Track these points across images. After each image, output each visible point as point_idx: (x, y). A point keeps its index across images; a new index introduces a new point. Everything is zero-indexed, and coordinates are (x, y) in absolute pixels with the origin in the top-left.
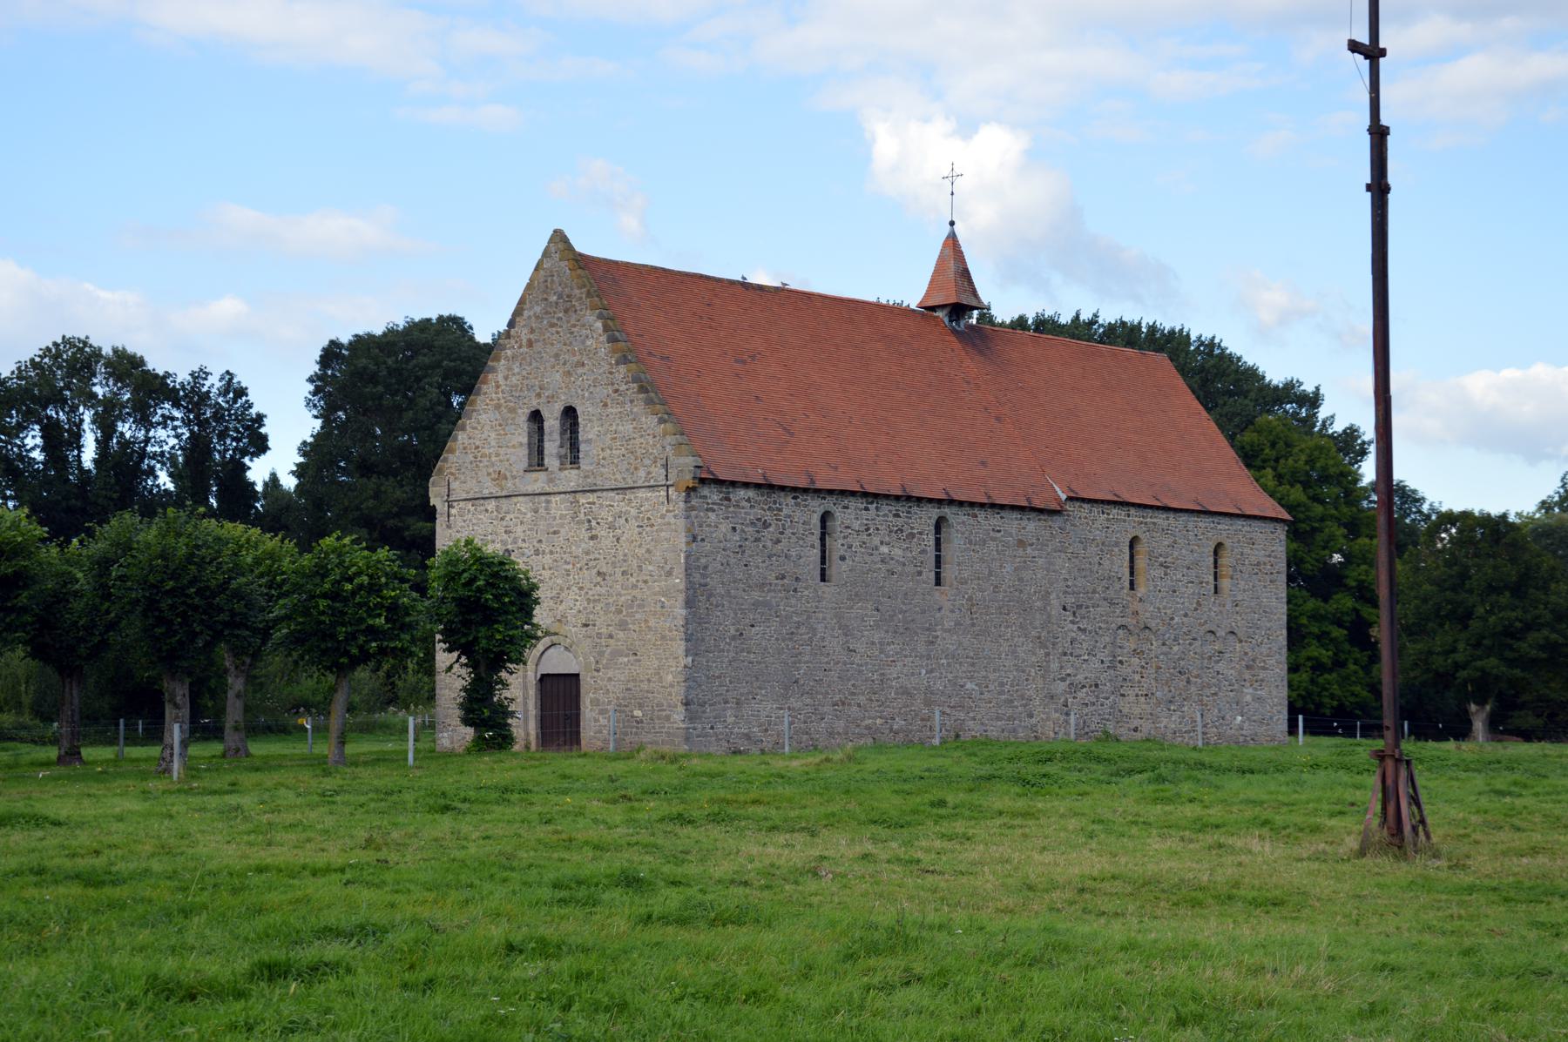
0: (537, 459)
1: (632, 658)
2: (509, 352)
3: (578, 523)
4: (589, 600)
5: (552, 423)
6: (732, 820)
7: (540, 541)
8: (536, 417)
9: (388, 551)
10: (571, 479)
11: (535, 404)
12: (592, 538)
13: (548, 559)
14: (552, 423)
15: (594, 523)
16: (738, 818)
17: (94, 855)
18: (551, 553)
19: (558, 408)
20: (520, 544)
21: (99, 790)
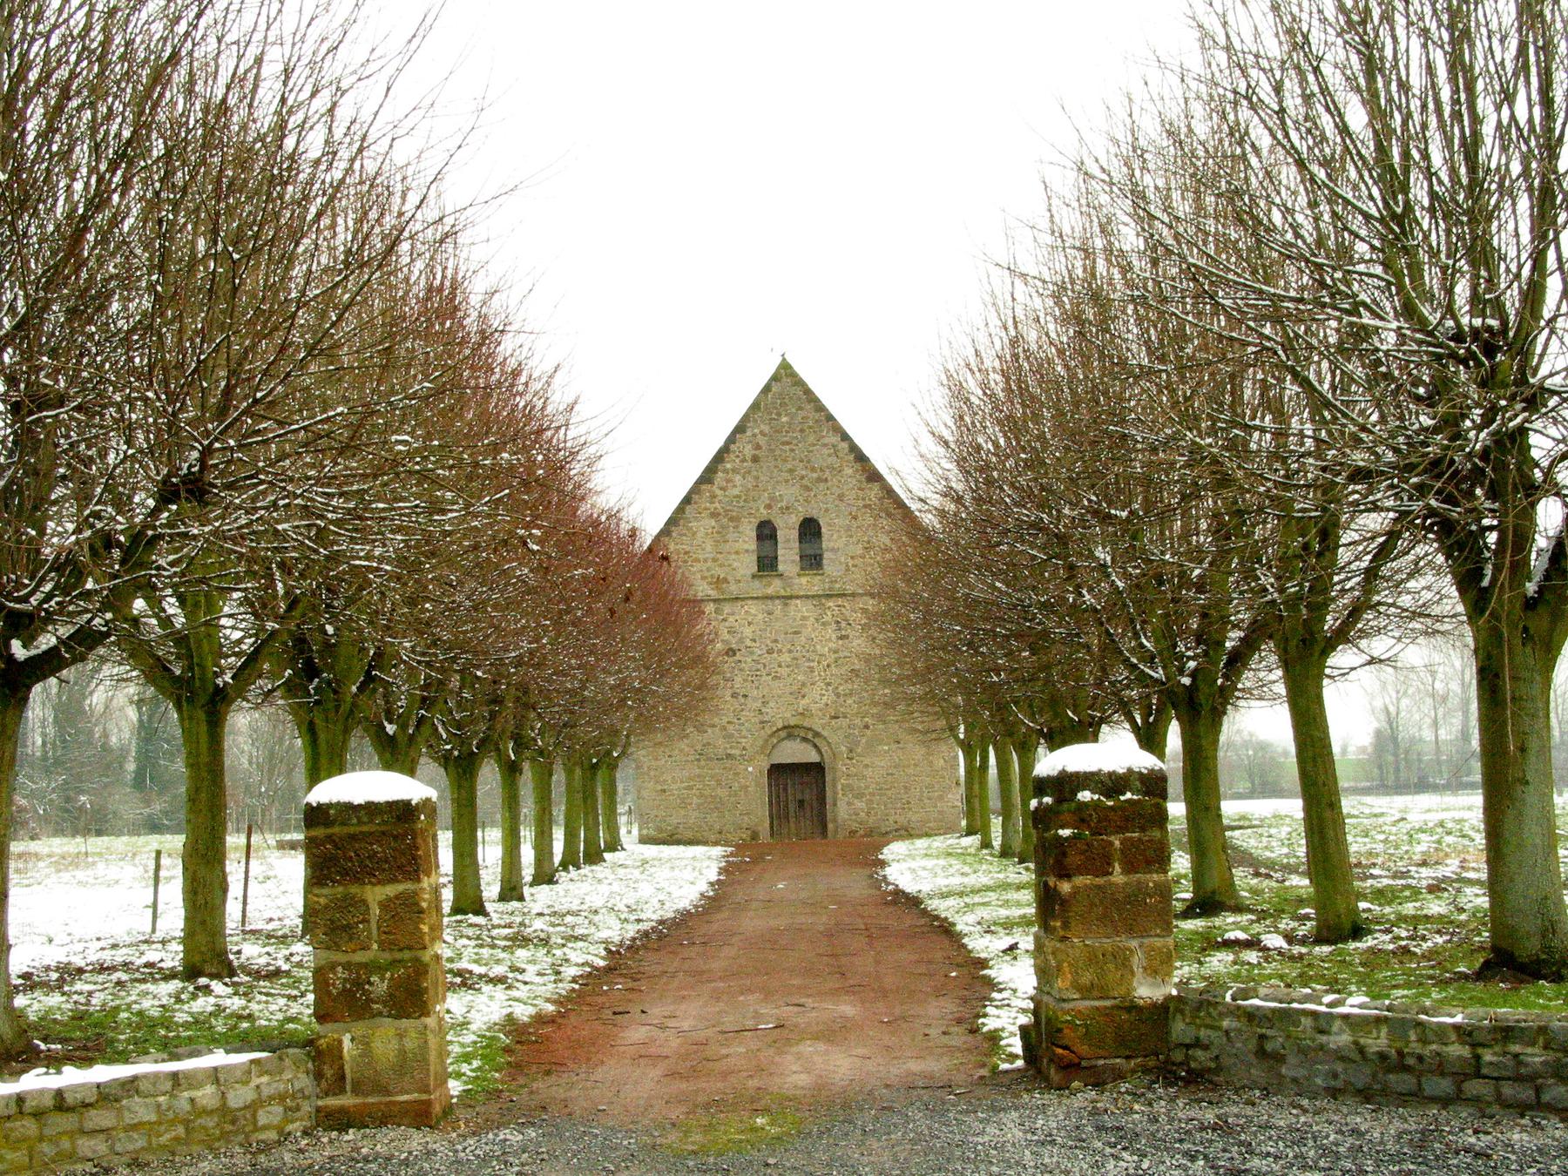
0: (767, 564)
1: (894, 746)
2: (728, 466)
3: (824, 624)
4: (838, 695)
5: (788, 535)
6: (306, 197)
7: (776, 641)
8: (766, 532)
9: (190, 466)
10: (807, 583)
11: (764, 514)
12: (841, 638)
13: (786, 658)
14: (788, 535)
15: (843, 624)
16: (454, 280)
17: (70, 1099)
18: (790, 651)
19: (795, 520)
20: (749, 643)
21: (1369, 910)
